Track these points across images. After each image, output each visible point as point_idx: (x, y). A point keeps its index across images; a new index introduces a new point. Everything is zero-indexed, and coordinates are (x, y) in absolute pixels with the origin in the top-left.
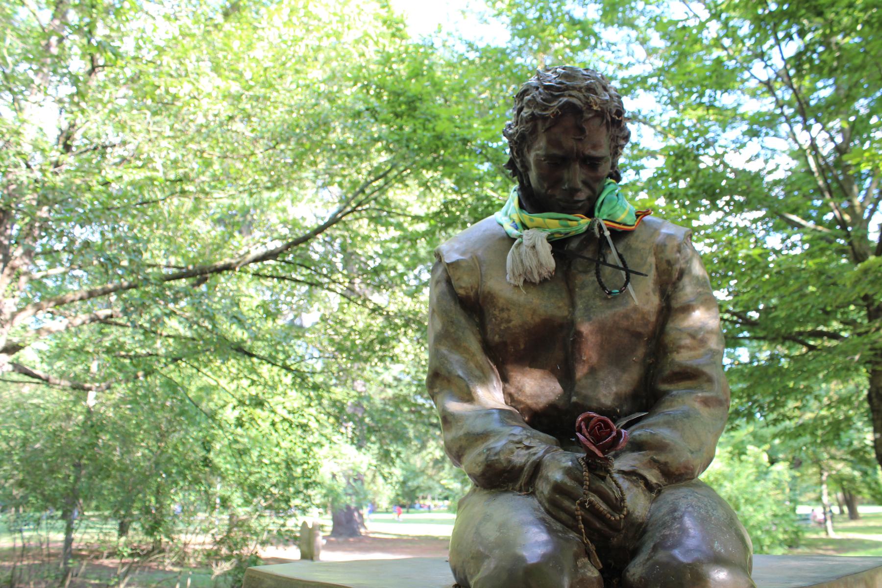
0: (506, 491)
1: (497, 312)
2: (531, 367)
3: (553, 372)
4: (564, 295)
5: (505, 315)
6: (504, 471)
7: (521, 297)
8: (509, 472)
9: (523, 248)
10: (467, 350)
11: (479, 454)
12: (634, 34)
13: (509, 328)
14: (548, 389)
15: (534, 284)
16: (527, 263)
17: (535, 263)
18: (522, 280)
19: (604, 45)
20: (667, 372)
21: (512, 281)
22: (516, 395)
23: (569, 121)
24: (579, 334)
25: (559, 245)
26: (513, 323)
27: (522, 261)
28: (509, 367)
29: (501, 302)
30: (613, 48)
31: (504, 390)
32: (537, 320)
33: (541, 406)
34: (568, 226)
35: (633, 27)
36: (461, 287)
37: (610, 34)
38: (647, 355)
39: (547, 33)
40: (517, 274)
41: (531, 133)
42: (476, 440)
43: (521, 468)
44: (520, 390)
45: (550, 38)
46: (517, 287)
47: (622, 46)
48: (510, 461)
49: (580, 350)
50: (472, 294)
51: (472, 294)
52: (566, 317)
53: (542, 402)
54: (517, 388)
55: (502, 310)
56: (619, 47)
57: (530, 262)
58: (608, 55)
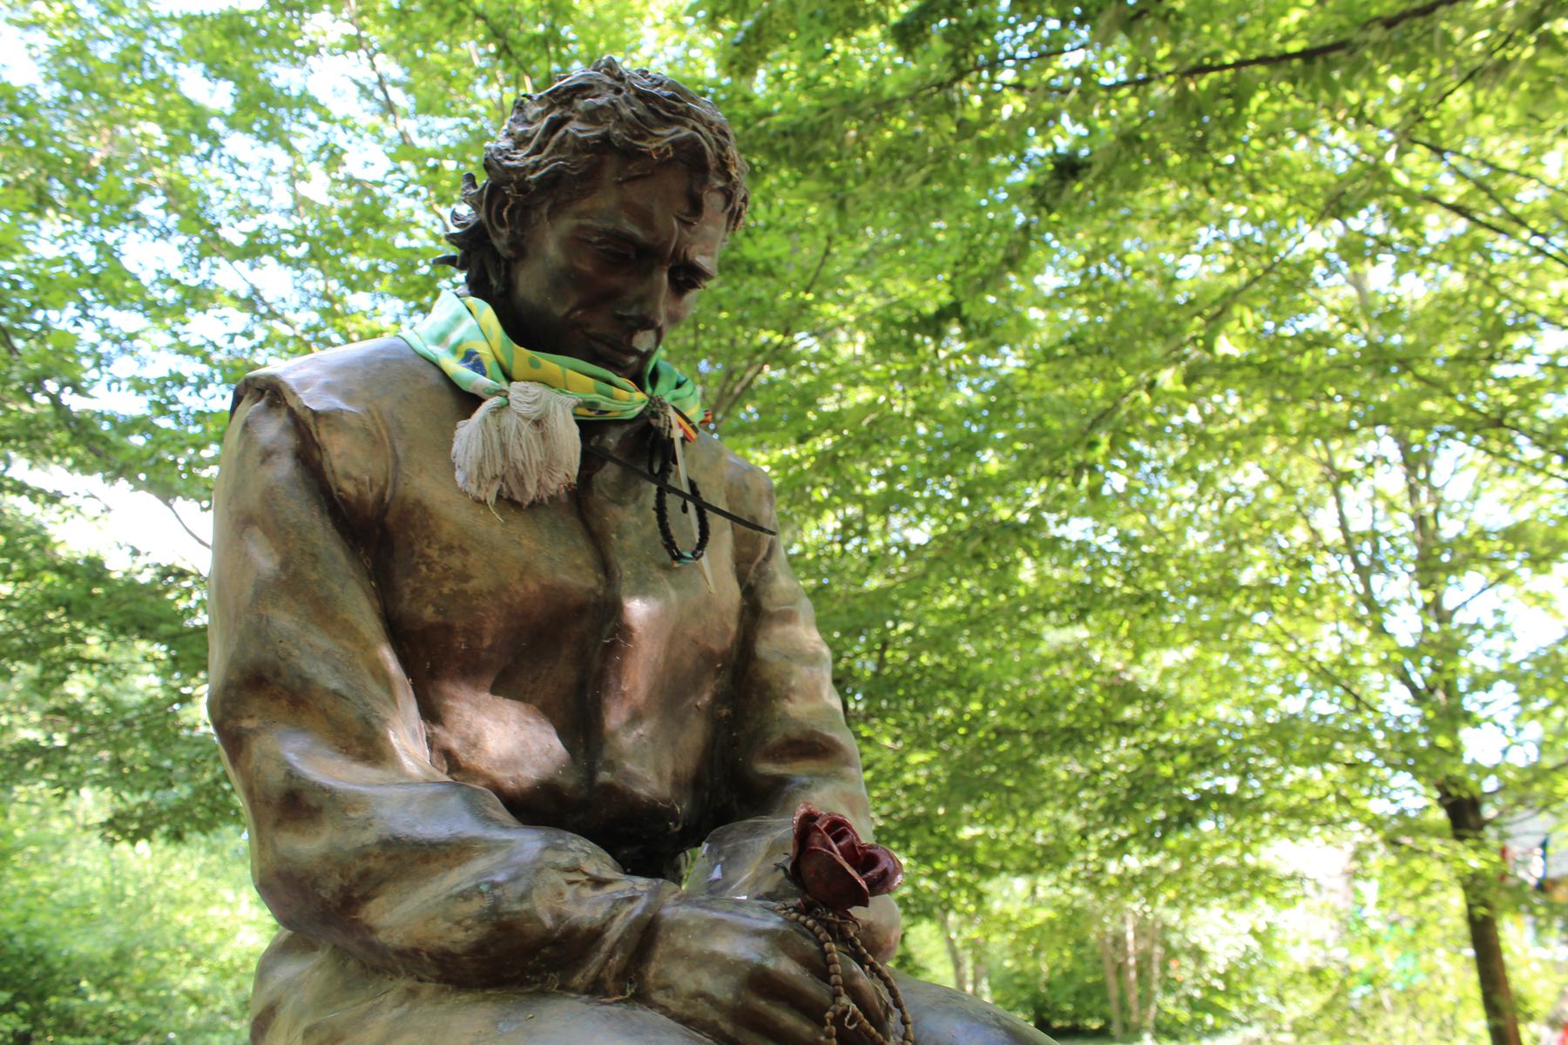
0: (543, 993)
1: (434, 553)
2: (495, 690)
3: (548, 711)
4: (581, 542)
5: (455, 561)
6: (547, 939)
7: (494, 527)
8: (556, 943)
9: (509, 420)
10: (349, 631)
11: (465, 896)
12: (282, 160)
13: (463, 592)
14: (535, 748)
15: (517, 505)
16: (517, 454)
17: (537, 457)
18: (495, 488)
19: (225, 161)
20: (776, 739)
21: (472, 488)
22: (463, 757)
23: (675, 182)
24: (624, 631)
25: (591, 428)
26: (473, 584)
27: (503, 446)
28: (448, 688)
29: (447, 532)
30: (240, 171)
31: (431, 742)
32: (533, 586)
33: (525, 785)
34: (610, 396)
35: (290, 149)
36: (348, 476)
37: (238, 144)
38: (718, 699)
39: (133, 98)
40: (488, 474)
41: (583, 177)
42: (426, 859)
43: (595, 936)
44: (474, 744)
45: (139, 110)
46: (481, 502)
47: (257, 172)
48: (559, 917)
49: (619, 669)
50: (371, 496)
51: (371, 496)
52: (592, 591)
53: (530, 774)
54: (465, 739)
55: (448, 549)
56: (251, 173)
57: (526, 450)
58: (229, 181)
